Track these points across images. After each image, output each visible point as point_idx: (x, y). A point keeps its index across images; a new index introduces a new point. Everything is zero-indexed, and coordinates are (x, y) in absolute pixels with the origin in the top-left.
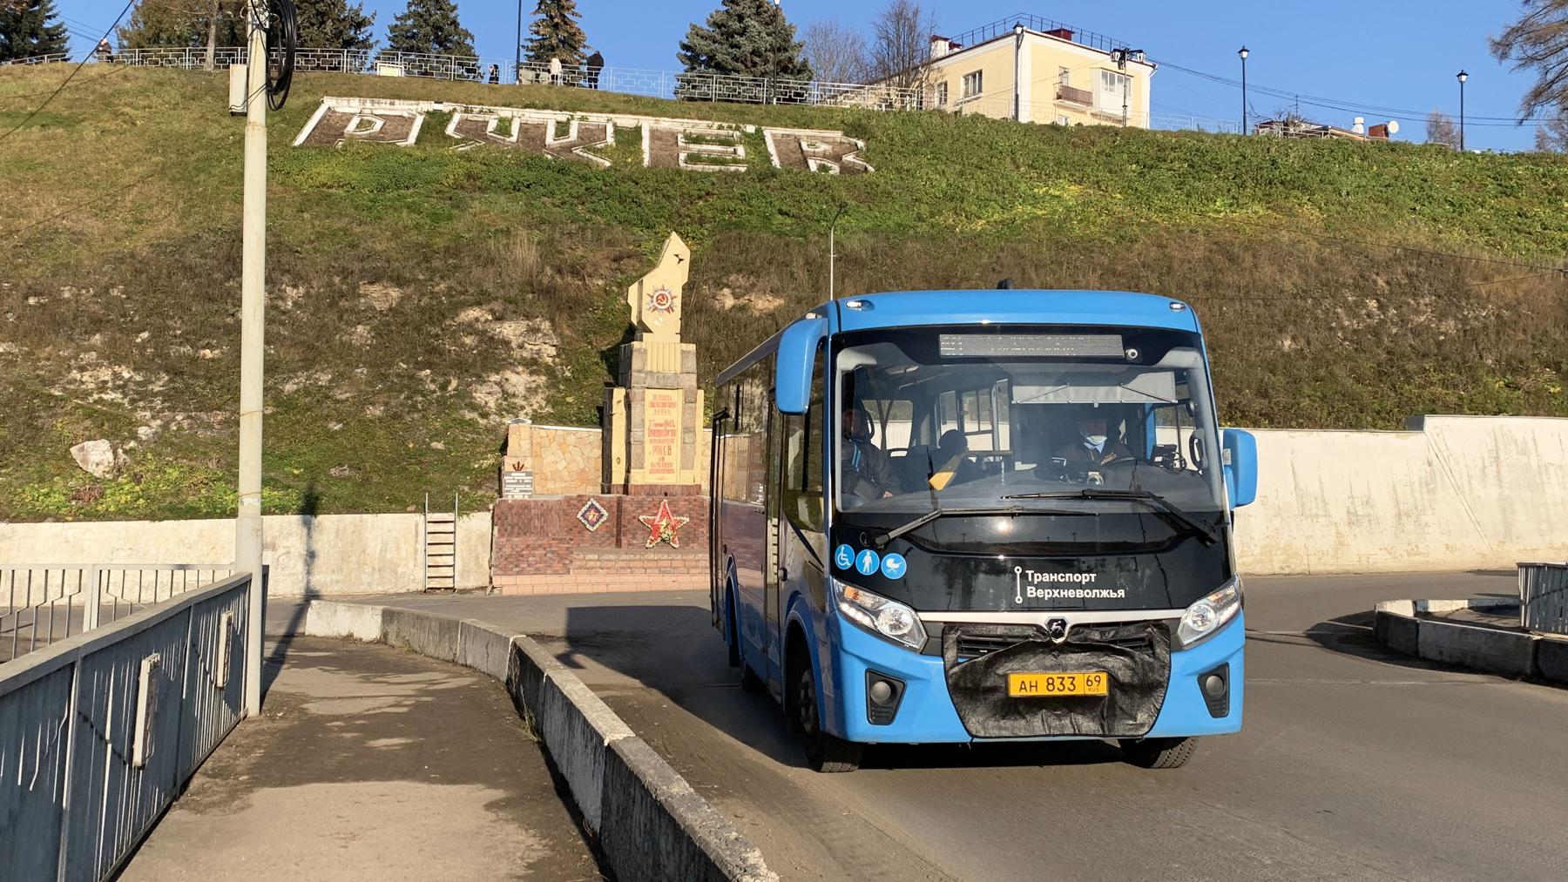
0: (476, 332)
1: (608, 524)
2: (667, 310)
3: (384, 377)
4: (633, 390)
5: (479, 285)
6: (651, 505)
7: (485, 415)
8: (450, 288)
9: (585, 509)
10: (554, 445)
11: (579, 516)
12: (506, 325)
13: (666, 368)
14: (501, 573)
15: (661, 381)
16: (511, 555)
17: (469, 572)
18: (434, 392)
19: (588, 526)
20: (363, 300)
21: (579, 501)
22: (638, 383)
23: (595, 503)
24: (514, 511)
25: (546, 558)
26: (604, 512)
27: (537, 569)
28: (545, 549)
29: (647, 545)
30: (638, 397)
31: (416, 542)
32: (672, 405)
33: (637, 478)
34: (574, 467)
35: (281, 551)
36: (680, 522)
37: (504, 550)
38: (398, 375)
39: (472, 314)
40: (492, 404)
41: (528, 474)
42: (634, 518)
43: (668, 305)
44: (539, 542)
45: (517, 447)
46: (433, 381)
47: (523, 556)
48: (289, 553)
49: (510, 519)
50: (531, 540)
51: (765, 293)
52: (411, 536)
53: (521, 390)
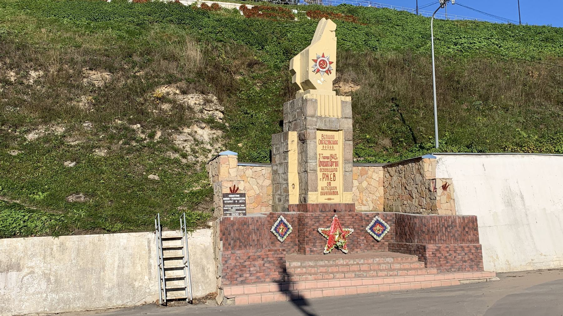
0: (169, 101)
1: (292, 235)
2: (326, 72)
3: (105, 129)
4: (308, 130)
5: (167, 72)
6: (325, 220)
7: (184, 156)
8: (146, 74)
9: (276, 224)
11: (272, 230)
12: (190, 96)
13: (331, 115)
14: (228, 283)
15: (328, 124)
16: (235, 266)
17: (197, 282)
18: (145, 139)
19: (279, 238)
20: (85, 80)
21: (271, 218)
22: (311, 125)
23: (283, 219)
24: (235, 227)
25: (264, 268)
26: (290, 226)
27: (258, 278)
28: (263, 259)
29: (325, 252)
30: (312, 136)
31: (150, 257)
32: (336, 143)
33: (313, 198)
35: (26, 271)
36: (349, 232)
37: (230, 262)
38: (116, 128)
39: (162, 90)
40: (188, 149)
42: (314, 230)
43: (327, 69)
44: (258, 254)
45: (227, 175)
46: (143, 132)
47: (245, 267)
48: (34, 272)
49: (232, 234)
50: (251, 251)
51: (348, 82)
52: (144, 253)
53: (206, 138)
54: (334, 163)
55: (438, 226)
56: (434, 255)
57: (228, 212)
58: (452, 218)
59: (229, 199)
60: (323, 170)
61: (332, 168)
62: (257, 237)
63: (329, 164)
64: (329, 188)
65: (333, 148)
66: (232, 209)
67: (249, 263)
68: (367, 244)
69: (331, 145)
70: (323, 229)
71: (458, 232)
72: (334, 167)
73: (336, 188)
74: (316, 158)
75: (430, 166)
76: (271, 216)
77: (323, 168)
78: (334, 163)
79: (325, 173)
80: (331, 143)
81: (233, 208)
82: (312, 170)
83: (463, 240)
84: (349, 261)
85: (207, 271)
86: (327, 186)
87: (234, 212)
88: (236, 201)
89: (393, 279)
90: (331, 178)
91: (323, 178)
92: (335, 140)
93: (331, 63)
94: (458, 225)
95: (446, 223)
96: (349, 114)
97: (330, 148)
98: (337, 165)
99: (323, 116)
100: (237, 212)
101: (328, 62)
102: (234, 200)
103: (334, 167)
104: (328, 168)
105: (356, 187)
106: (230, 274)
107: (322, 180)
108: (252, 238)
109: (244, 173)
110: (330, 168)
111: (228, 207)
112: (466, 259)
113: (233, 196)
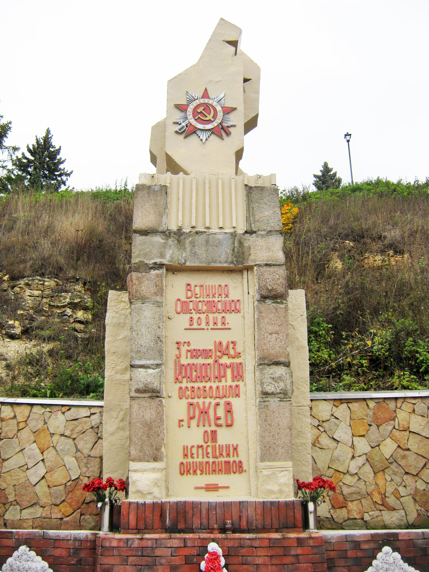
10: (25, 434)
15: (201, 252)
43: (215, 124)
54: (229, 371)
60: (189, 393)
61: (220, 384)
63: (213, 372)
64: (210, 450)
69: (216, 315)
72: (229, 382)
73: (235, 449)
74: (160, 353)
77: (190, 385)
78: (229, 371)
79: (195, 401)
82: (145, 391)
86: (202, 443)
90: (219, 418)
91: (192, 418)
93: (228, 111)
96: (271, 221)
99: (186, 230)
101: (219, 108)
103: (228, 381)
104: (208, 385)
105: (364, 457)
107: (185, 423)
109: (45, 423)
110: (214, 385)
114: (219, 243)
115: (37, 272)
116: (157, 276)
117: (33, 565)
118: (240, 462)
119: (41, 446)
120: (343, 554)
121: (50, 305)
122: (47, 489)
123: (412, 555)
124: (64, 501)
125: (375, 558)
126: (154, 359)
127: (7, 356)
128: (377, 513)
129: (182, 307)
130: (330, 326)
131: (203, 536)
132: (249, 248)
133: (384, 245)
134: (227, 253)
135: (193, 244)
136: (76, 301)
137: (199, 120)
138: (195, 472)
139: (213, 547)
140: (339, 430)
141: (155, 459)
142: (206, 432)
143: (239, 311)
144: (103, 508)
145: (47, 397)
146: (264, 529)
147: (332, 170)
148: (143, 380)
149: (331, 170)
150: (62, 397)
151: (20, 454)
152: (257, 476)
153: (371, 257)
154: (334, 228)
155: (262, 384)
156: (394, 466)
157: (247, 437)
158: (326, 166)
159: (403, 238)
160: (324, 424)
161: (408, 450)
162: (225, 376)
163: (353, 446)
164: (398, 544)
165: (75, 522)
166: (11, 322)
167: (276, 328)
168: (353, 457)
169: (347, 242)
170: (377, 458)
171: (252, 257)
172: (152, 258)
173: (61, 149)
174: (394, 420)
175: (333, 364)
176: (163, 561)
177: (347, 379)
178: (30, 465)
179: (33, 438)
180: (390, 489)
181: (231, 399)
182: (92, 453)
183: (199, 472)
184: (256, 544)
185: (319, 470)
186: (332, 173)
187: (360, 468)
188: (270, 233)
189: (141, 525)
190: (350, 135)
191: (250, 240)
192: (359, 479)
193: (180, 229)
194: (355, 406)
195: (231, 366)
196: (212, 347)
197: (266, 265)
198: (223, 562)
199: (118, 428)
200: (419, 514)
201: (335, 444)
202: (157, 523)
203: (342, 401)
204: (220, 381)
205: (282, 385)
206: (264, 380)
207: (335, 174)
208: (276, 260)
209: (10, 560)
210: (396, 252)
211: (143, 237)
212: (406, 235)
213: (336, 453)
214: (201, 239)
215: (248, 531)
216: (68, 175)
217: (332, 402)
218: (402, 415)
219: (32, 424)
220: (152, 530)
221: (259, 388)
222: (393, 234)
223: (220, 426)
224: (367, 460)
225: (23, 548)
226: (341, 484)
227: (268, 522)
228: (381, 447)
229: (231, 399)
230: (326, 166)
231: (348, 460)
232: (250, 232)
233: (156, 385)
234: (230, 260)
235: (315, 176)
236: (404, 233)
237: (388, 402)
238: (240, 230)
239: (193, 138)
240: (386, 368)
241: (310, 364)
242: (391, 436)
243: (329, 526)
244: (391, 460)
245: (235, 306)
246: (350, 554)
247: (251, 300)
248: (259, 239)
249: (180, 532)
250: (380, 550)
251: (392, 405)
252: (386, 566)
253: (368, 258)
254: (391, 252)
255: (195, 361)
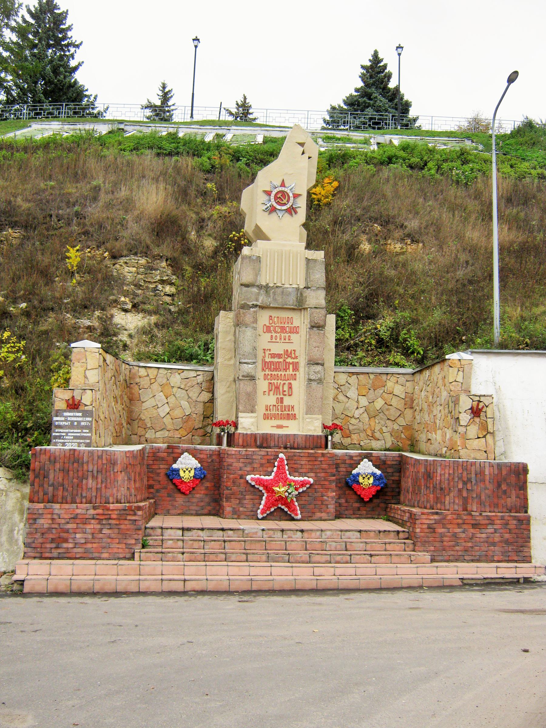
6: (263, 461)
10: (155, 386)
15: (279, 298)
16: (50, 529)
25: (101, 536)
32: (295, 330)
34: (178, 413)
41: (86, 414)
43: (288, 206)
45: (82, 380)
49: (51, 476)
54: (291, 366)
55: (451, 478)
56: (432, 530)
57: (59, 441)
58: (478, 465)
59: (63, 419)
60: (269, 377)
61: (286, 373)
62: (97, 485)
63: (282, 366)
64: (279, 407)
65: (289, 339)
66: (67, 435)
67: (75, 526)
68: (346, 504)
69: (286, 334)
70: (253, 476)
71: (487, 491)
73: (293, 407)
74: (255, 356)
75: (461, 373)
76: (170, 450)
77: (270, 373)
78: (291, 366)
79: (273, 381)
80: (286, 332)
81: (69, 434)
82: (247, 377)
83: (496, 505)
84: (274, 534)
85: (18, 533)
86: (275, 404)
87: (71, 441)
88: (76, 423)
89: (333, 569)
90: (285, 391)
91: (270, 391)
92: (293, 325)
93: (296, 196)
94: (487, 478)
95: (465, 473)
96: (319, 281)
97: (285, 339)
98: (296, 368)
100: (75, 441)
101: (291, 195)
102: (72, 422)
104: (280, 373)
105: (364, 408)
106: (41, 540)
107: (267, 393)
108: (87, 484)
111: (60, 432)
112: (497, 540)
113: (71, 414)
114: (289, 294)
115: (131, 251)
116: (254, 312)
117: (191, 462)
118: (295, 414)
119: (166, 394)
120: (344, 462)
121: (144, 281)
122: (170, 420)
123: (378, 463)
124: (181, 427)
125: (359, 464)
126: (252, 359)
127: (127, 327)
128: (369, 441)
129: (267, 329)
130: (353, 312)
131: (276, 450)
132: (306, 297)
133: (404, 234)
134: (293, 300)
135: (274, 293)
136: (164, 278)
137: (278, 203)
138: (271, 418)
139: (281, 455)
140: (350, 391)
141: (252, 412)
142: (278, 398)
143: (298, 333)
144: (224, 435)
145: (165, 362)
146: (305, 448)
147: (382, 61)
148: (246, 371)
149: (382, 60)
150: (174, 362)
151: (153, 399)
152: (303, 422)
153: (392, 244)
154: (366, 209)
155: (309, 374)
156: (381, 415)
157: (299, 402)
158: (376, 55)
159: (420, 228)
160: (342, 387)
161: (391, 405)
162: (289, 368)
163: (358, 402)
164: (372, 458)
165: (189, 440)
166: (123, 299)
167: (318, 344)
168: (357, 408)
169: (376, 225)
170: (371, 410)
171: (307, 303)
172: (252, 301)
173: (69, 13)
174: (384, 386)
175: (352, 342)
176: (257, 461)
177: (361, 354)
178: (159, 406)
179: (160, 389)
180: (377, 428)
181: (292, 382)
182: (198, 400)
183: (273, 418)
184: (302, 455)
185: (336, 414)
186: (382, 64)
187: (361, 415)
188: (318, 288)
189: (245, 444)
190: (402, 48)
191: (307, 292)
192: (360, 421)
193: (267, 285)
194: (361, 377)
195: (293, 363)
196: (283, 353)
197: (315, 308)
198: (286, 462)
199: (226, 392)
200: (393, 443)
201: (347, 400)
202: (253, 443)
203: (353, 373)
204: (286, 371)
205: (319, 376)
206: (310, 373)
207: (385, 66)
208: (321, 305)
209: (179, 459)
210: (413, 241)
211: (246, 288)
212: (423, 226)
213: (347, 405)
214: (279, 291)
215: (298, 449)
216: (78, 46)
217: (347, 374)
218: (390, 384)
219: (159, 380)
220: (251, 447)
221: (307, 376)
222: (412, 224)
223: (285, 395)
224: (366, 410)
225: (186, 454)
226: (348, 423)
227: (308, 445)
228: (375, 403)
229: (292, 382)
230: (376, 55)
231: (354, 410)
232: (307, 288)
233: (253, 373)
234: (295, 304)
235: (363, 67)
236: (422, 223)
237: (382, 375)
238: (302, 287)
239: (274, 215)
240: (387, 347)
241: (336, 340)
242: (381, 397)
243: (340, 447)
244: (380, 411)
245: (296, 330)
246: (347, 462)
247: (305, 327)
248: (312, 292)
249: (264, 448)
250: (362, 460)
251: (384, 377)
252: (364, 468)
253: (390, 244)
254: (409, 241)
255: (273, 360)
